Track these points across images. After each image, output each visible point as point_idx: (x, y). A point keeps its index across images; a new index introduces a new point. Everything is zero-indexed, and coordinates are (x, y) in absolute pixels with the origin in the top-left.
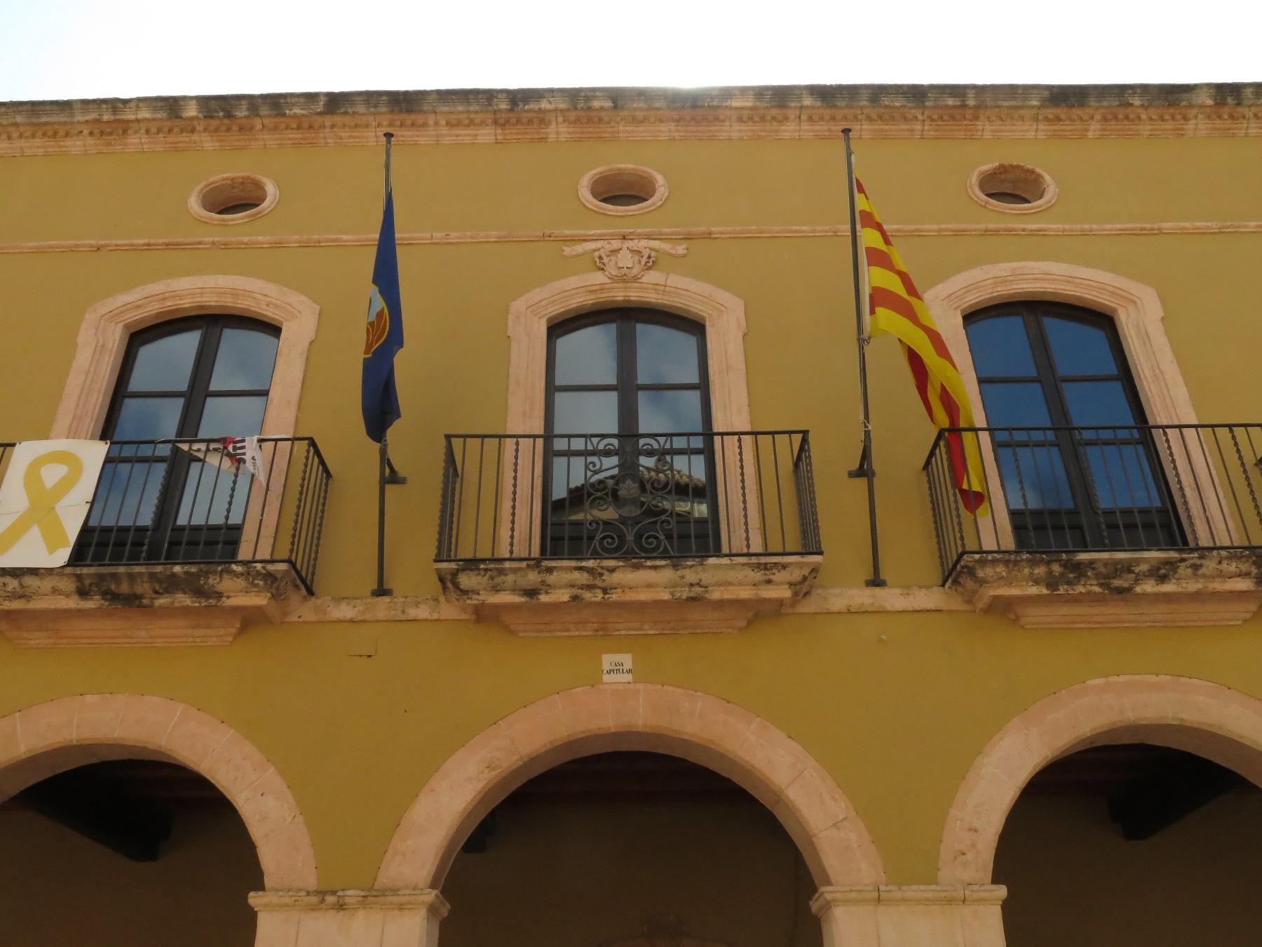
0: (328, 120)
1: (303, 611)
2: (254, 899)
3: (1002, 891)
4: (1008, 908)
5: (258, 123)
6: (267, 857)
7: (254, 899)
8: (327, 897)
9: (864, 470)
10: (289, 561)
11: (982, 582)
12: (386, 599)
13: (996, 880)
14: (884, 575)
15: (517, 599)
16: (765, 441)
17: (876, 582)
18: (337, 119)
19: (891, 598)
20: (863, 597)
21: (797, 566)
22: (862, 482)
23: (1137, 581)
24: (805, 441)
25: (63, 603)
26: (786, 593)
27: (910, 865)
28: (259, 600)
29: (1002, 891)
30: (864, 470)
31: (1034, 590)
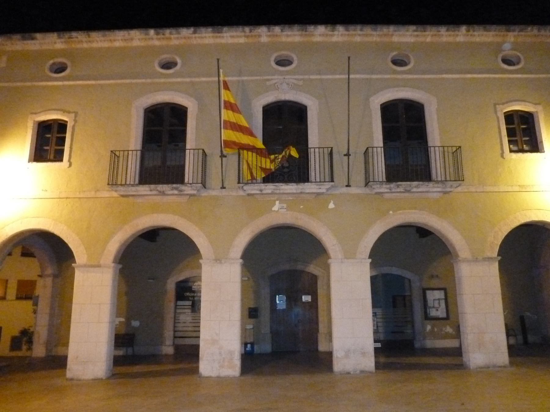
0: (194, 36)
1: (204, 193)
2: (201, 261)
3: (370, 260)
4: (371, 263)
5: (172, 36)
6: (202, 251)
7: (201, 261)
8: (218, 260)
9: (348, 155)
10: (202, 183)
11: (374, 188)
12: (224, 190)
13: (370, 257)
14: (351, 184)
15: (258, 192)
16: (321, 150)
17: (348, 186)
18: (197, 35)
19: (353, 190)
20: (345, 190)
21: (328, 185)
22: (347, 157)
23: (412, 188)
24: (331, 150)
25: (145, 193)
26: (324, 191)
27: (350, 254)
28: (195, 192)
29: (370, 260)
30: (348, 155)
31: (386, 191)
